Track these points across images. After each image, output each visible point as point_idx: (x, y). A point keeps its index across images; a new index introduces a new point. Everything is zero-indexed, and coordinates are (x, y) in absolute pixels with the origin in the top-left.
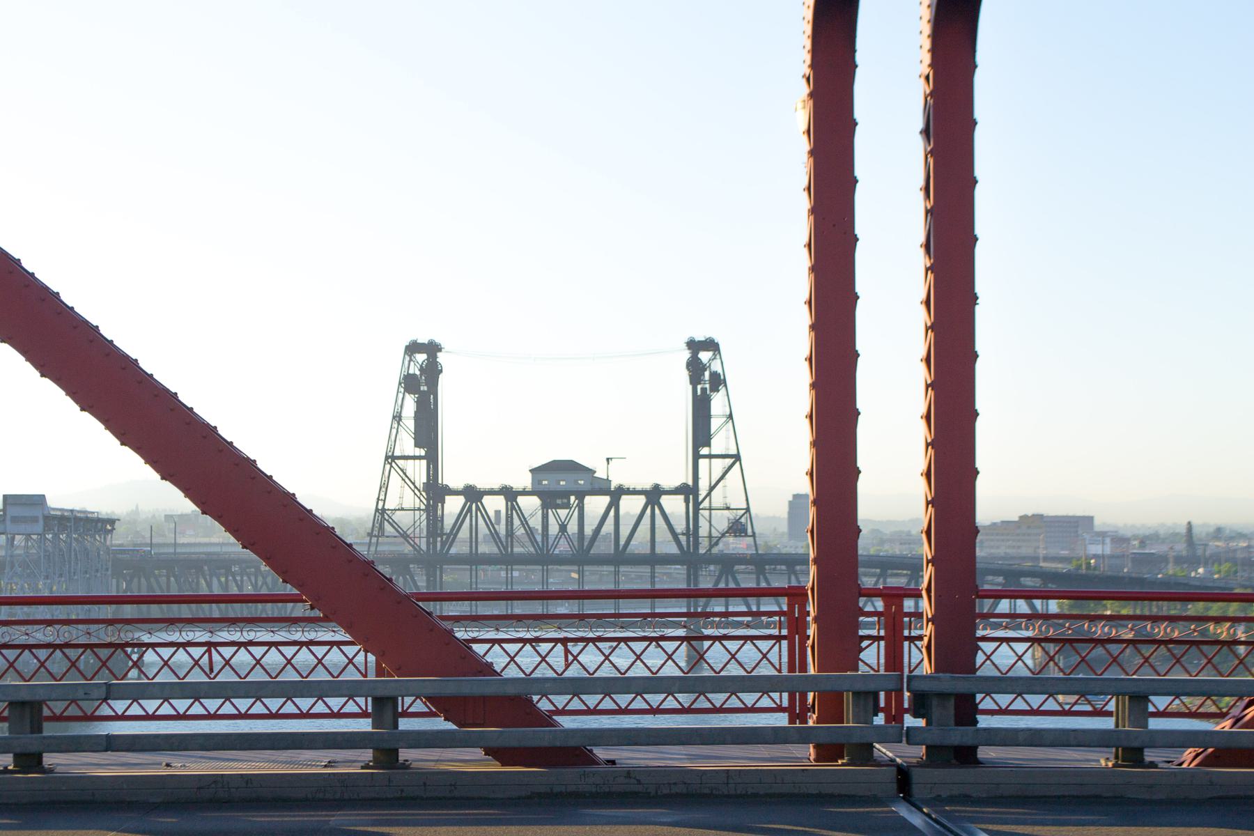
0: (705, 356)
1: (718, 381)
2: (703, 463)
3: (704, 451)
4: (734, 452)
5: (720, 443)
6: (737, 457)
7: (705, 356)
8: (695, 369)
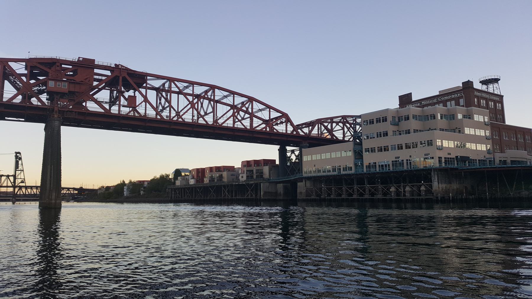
0: (18, 155)
1: (20, 159)
2: (17, 171)
3: (17, 170)
4: (22, 169)
5: (20, 168)
6: (23, 170)
7: (18, 155)
8: (16, 157)
